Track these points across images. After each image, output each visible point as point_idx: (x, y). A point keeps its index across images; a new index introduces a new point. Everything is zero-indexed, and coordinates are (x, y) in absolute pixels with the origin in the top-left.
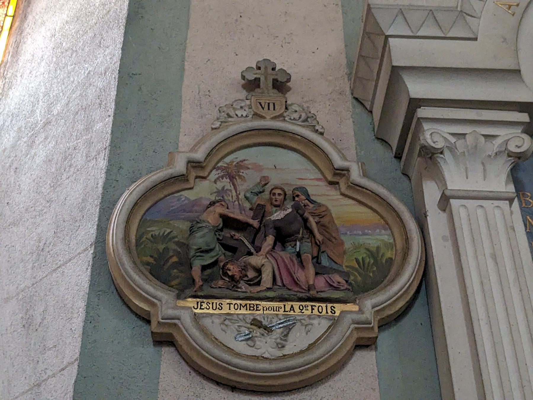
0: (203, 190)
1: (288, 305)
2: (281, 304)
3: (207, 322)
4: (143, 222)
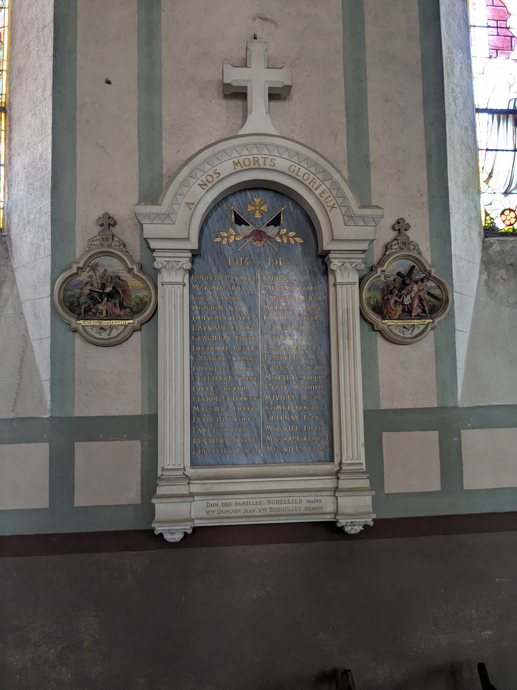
0: (84, 277)
1: (112, 321)
2: (109, 321)
3: (86, 328)
4: (65, 290)
